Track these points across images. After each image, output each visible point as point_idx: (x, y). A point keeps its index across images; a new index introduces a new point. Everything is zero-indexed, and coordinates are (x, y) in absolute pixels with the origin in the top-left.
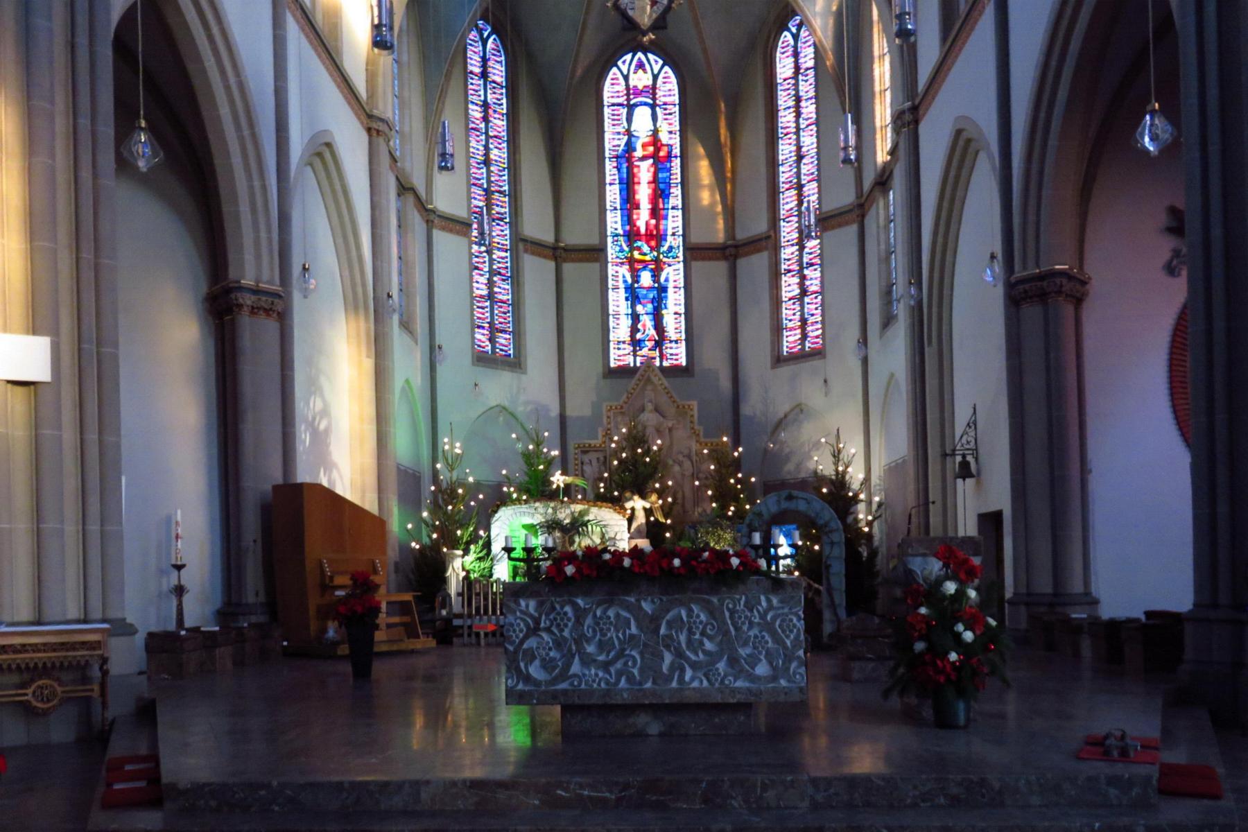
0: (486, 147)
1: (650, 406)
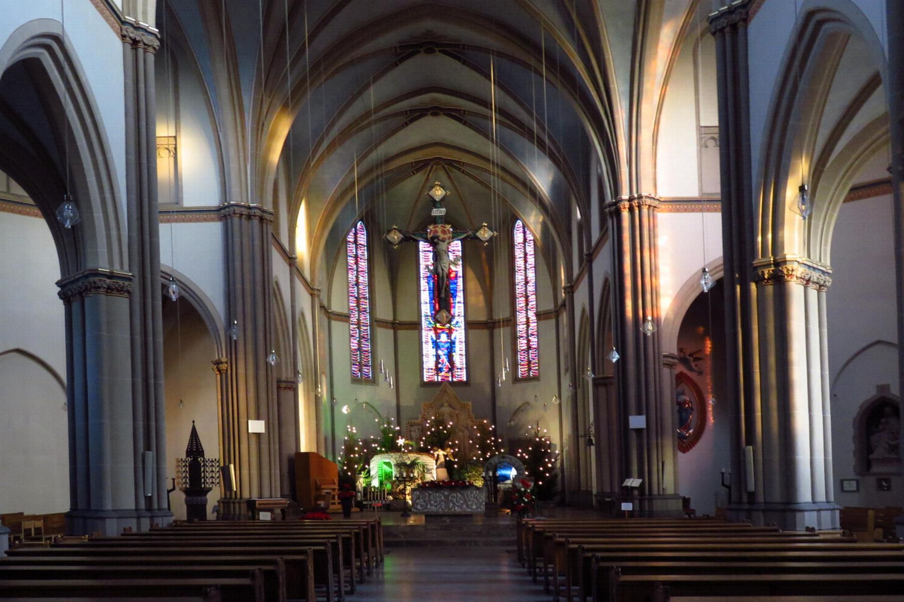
0: (357, 277)
1: (446, 404)
